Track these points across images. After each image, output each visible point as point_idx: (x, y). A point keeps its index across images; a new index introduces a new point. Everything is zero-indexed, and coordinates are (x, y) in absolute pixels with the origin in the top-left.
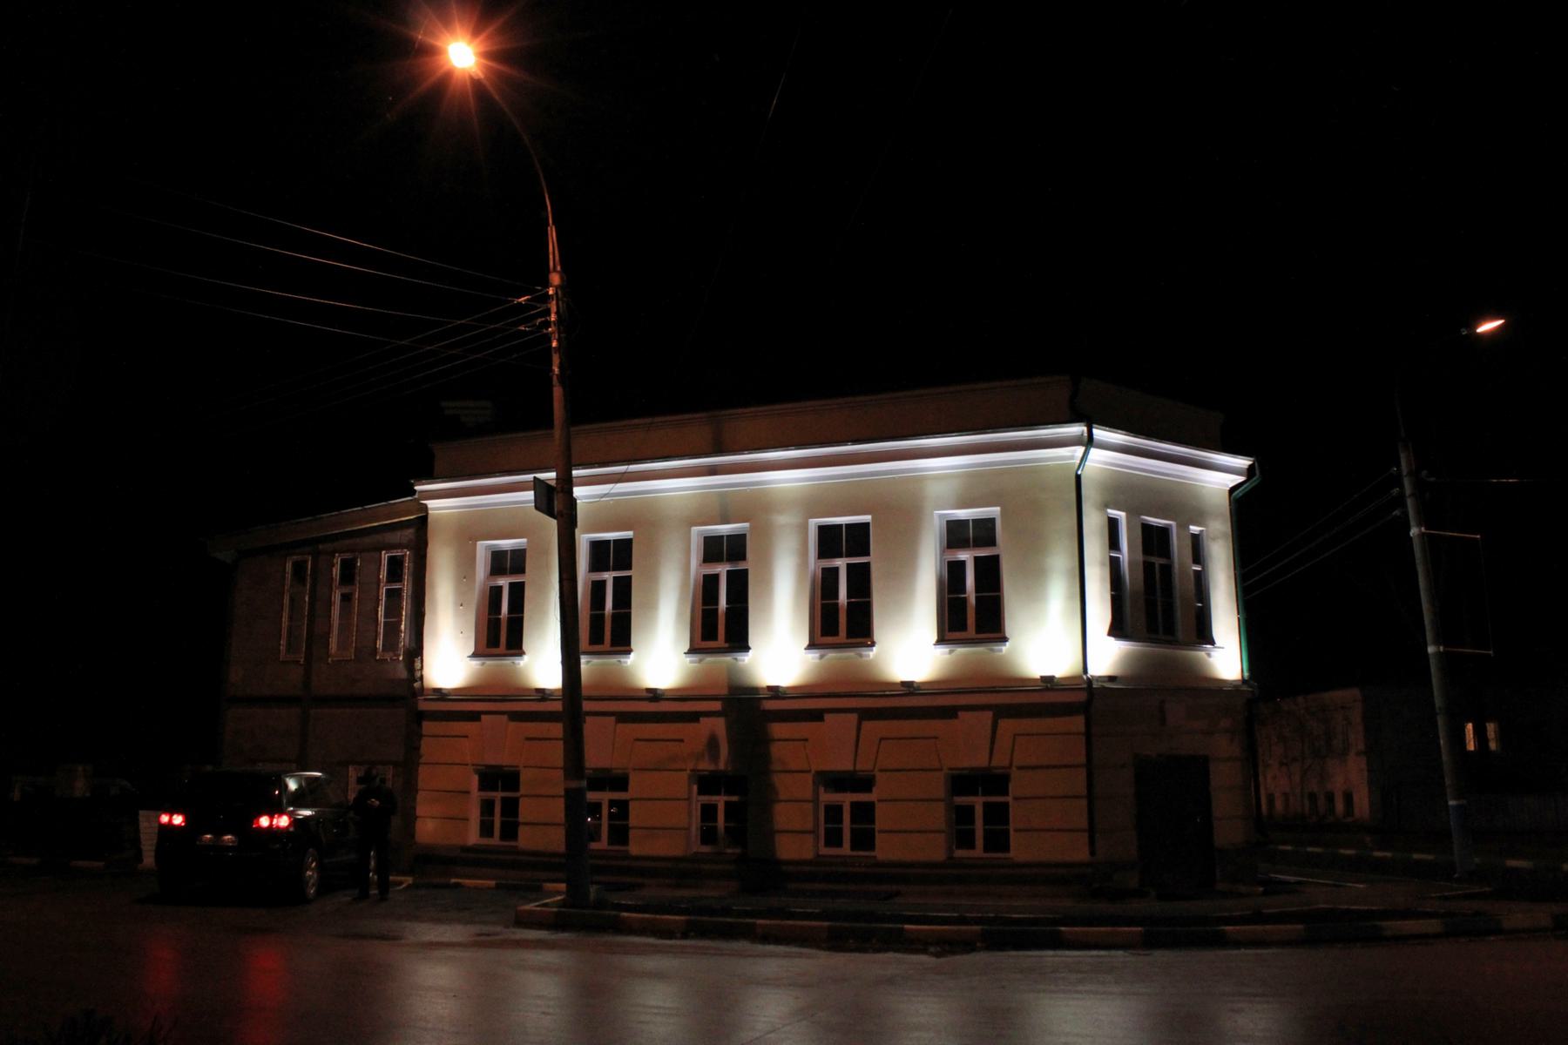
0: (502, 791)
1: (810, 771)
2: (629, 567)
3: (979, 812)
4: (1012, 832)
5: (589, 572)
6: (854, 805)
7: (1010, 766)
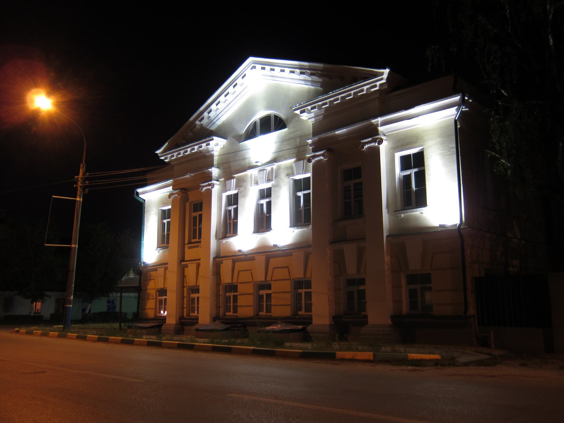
0: (305, 288)
5: (401, 171)
6: (233, 296)
7: (237, 283)
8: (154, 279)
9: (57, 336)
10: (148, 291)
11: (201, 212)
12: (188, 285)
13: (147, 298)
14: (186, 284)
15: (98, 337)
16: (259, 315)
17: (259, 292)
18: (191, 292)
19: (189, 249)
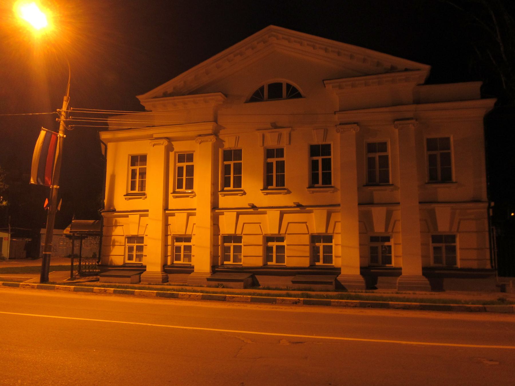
1: (124, 236)
2: (240, 159)
3: (135, 248)
4: (286, 257)
7: (333, 233)
8: (123, 226)
9: (112, 292)
10: (113, 238)
11: (283, 158)
12: (172, 234)
13: (111, 244)
14: (171, 233)
15: (74, 288)
16: (267, 265)
17: (267, 243)
18: (175, 240)
19: (174, 198)
